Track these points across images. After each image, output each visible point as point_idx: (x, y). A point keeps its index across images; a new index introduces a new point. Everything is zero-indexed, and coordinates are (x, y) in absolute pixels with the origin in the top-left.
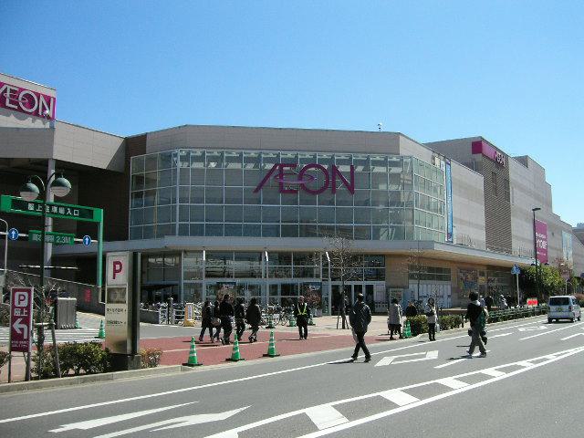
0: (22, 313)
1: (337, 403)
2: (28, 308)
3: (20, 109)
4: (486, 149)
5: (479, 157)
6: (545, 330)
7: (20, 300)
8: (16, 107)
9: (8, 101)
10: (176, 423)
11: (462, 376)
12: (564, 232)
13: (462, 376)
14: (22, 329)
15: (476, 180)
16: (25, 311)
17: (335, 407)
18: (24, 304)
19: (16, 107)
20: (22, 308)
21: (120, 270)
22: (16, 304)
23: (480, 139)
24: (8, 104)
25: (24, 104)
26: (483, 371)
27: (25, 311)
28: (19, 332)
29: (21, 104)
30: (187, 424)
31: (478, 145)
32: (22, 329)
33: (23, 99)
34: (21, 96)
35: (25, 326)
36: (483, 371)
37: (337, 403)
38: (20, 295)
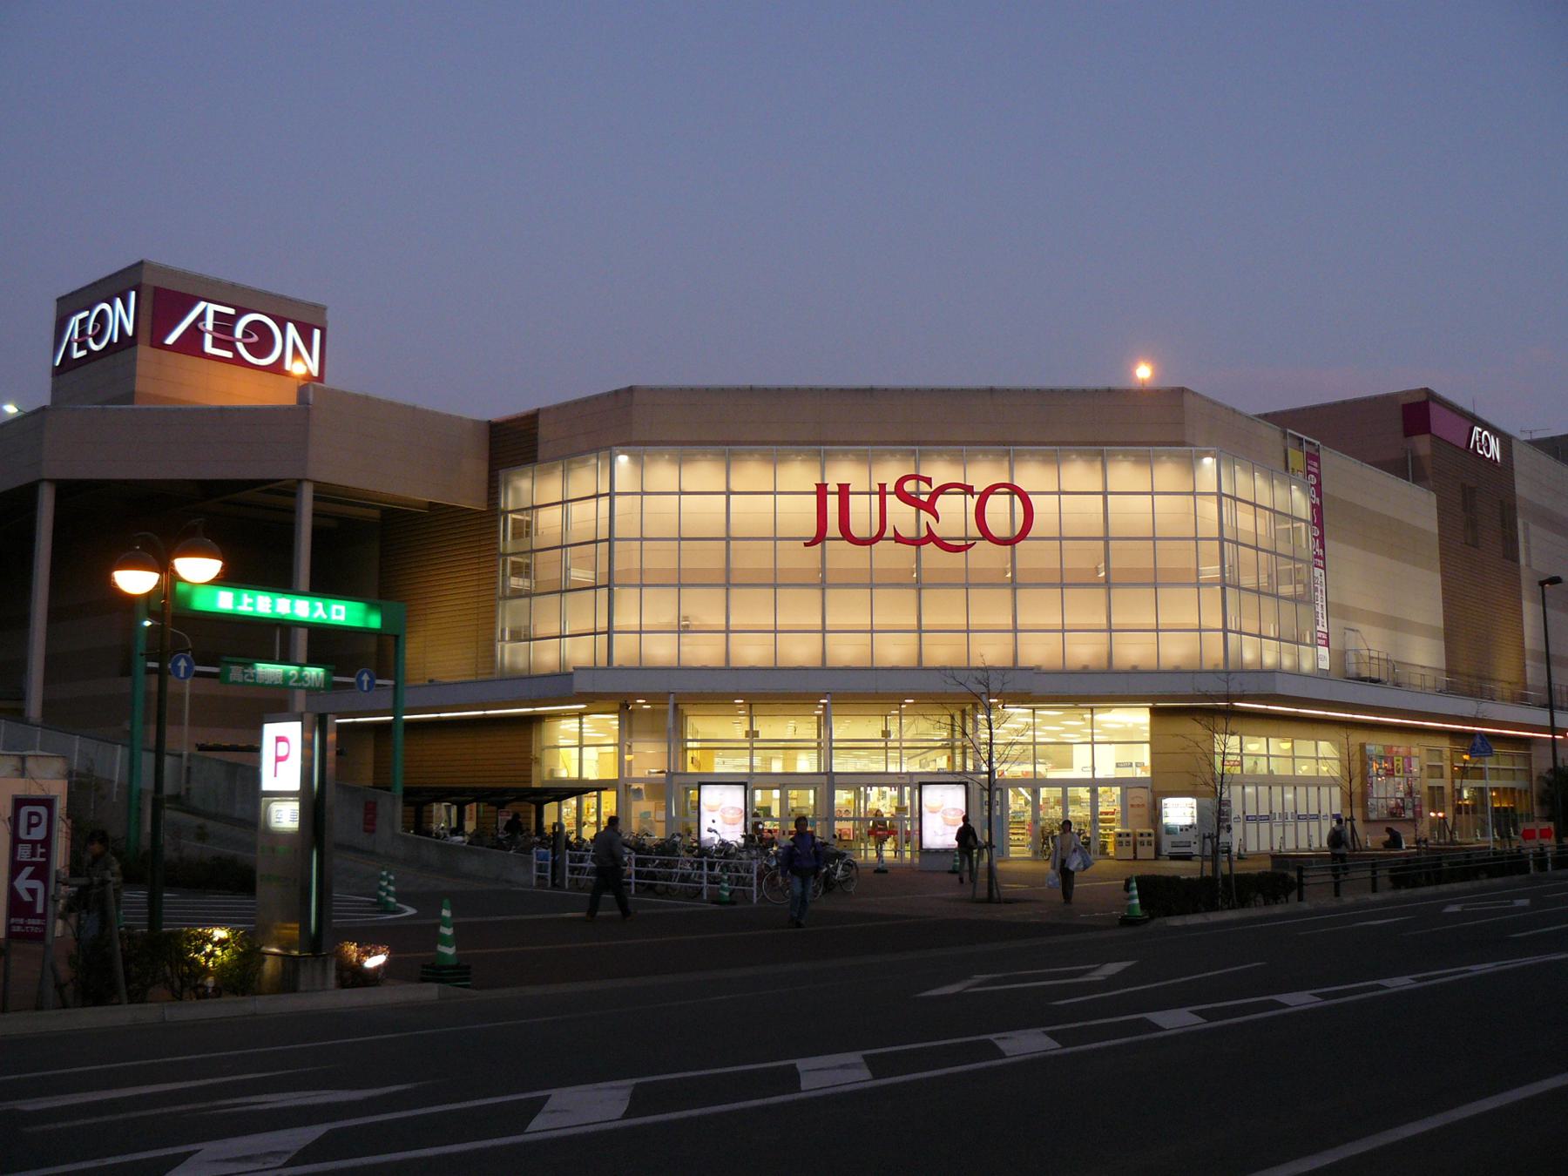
0: (33, 855)
1: (1000, 1062)
2: (47, 843)
3: (238, 360)
4: (1439, 421)
5: (1422, 444)
6: (1524, 908)
7: (30, 826)
8: (229, 354)
9: (208, 339)
10: (843, 1067)
11: (1276, 1012)
12: (549, 831)
13: (1276, 1012)
14: (33, 892)
15: (1419, 508)
16: (40, 850)
17: (1002, 1055)
18: (39, 834)
19: (229, 354)
20: (34, 843)
21: (36, 825)
22: (23, 835)
23: (1423, 397)
24: (208, 347)
25: (247, 346)
26: (1276, 997)
27: (40, 850)
28: (27, 898)
29: (240, 346)
30: (286, 1104)
31: (1417, 412)
32: (33, 892)
33: (246, 334)
34: (238, 333)
35: (37, 884)
36: (1276, 997)
37: (1000, 1062)
38: (30, 814)
